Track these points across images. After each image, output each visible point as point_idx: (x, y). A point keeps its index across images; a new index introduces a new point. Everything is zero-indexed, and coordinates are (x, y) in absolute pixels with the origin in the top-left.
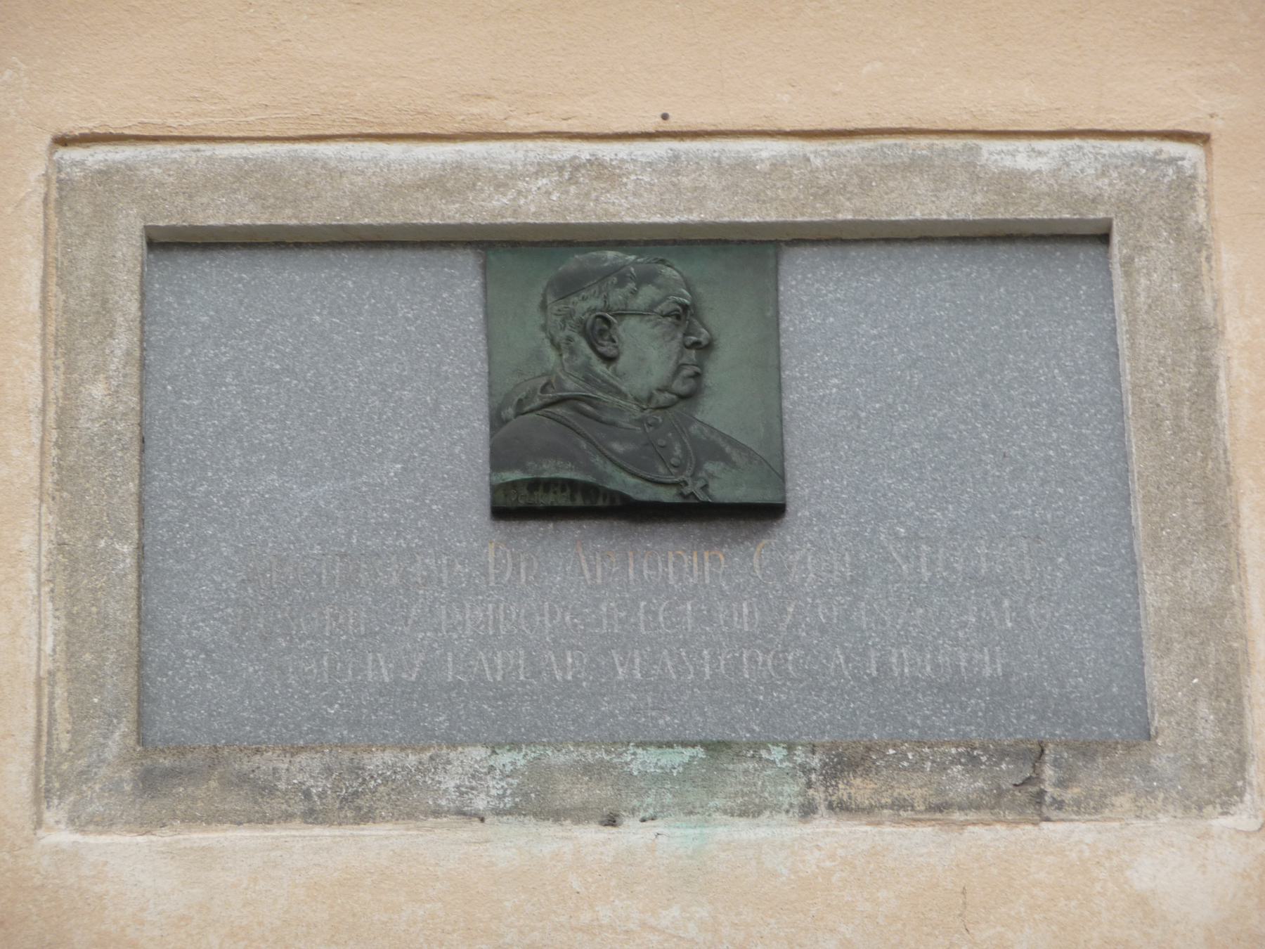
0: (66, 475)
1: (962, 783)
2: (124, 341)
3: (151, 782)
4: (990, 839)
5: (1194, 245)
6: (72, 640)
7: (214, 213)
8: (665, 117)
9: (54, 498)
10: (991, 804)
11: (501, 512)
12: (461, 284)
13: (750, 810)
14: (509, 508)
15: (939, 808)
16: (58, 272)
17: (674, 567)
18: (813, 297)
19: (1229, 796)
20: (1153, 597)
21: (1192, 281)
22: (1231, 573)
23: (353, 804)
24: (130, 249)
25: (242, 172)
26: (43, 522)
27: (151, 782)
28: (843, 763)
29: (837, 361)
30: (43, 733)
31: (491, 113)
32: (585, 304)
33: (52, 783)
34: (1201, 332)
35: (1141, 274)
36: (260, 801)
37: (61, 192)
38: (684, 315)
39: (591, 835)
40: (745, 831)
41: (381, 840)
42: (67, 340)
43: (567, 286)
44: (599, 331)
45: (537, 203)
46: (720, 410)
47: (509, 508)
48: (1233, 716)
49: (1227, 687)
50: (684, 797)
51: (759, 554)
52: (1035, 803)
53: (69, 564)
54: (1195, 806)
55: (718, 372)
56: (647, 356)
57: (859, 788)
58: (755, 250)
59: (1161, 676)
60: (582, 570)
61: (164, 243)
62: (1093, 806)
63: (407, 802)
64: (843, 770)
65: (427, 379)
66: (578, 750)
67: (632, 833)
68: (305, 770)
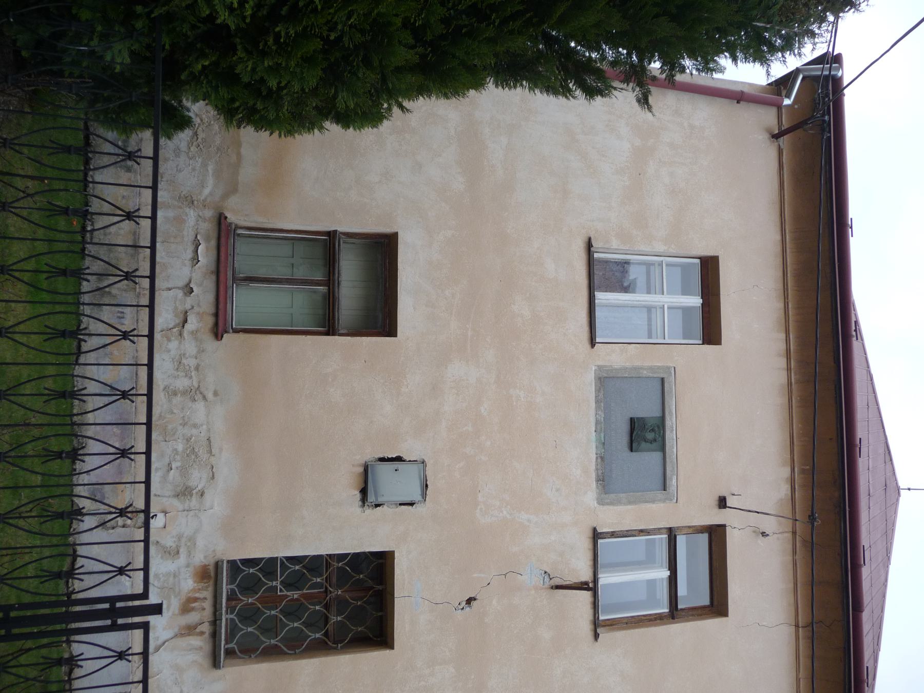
0: (636, 369)
1: (600, 472)
2: (651, 375)
3: (600, 379)
4: (594, 475)
5: (664, 501)
6: (616, 369)
7: (666, 385)
8: (722, 503)
9: (123, 197)
10: (597, 475)
11: (631, 419)
12: (658, 414)
13: (596, 447)
14: (632, 420)
15: (597, 469)
16: (659, 367)
17: (624, 439)
18: (657, 455)
19: (598, 503)
20: (622, 495)
21: (660, 500)
22: (625, 504)
23: (597, 402)
24: (662, 376)
25: (671, 389)
26: (146, 224)
27: (600, 379)
28: (602, 458)
29: (650, 458)
30: (606, 366)
31: (679, 418)
32: (656, 429)
33: (600, 368)
34: (653, 501)
35: (660, 494)
36: (598, 391)
37: (669, 368)
38: (655, 440)
39: (594, 429)
40: (594, 447)
41: (593, 405)
42: (651, 369)
43: (658, 427)
44: (653, 430)
45: (668, 423)
46: (643, 445)
47: (632, 420)
48: (608, 504)
49: (611, 504)
50: (598, 440)
51: (626, 449)
52: (598, 480)
53: (625, 369)
54: (597, 499)
55: (648, 445)
56: (650, 436)
57: (599, 460)
58: (663, 449)
59: (612, 496)
60: (624, 428)
61: (663, 380)
62: (597, 487)
63: (598, 408)
64: (601, 458)
65: (647, 410)
66: (603, 427)
67: (594, 434)
68: (601, 395)
